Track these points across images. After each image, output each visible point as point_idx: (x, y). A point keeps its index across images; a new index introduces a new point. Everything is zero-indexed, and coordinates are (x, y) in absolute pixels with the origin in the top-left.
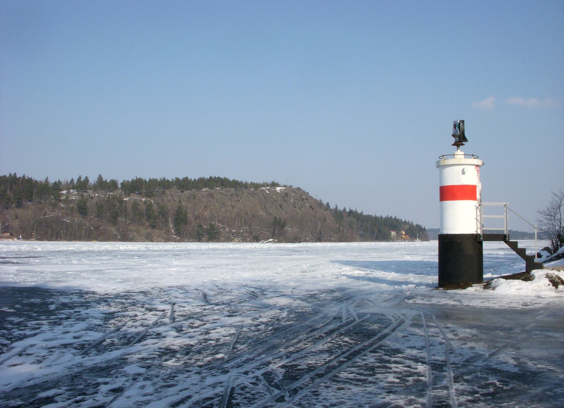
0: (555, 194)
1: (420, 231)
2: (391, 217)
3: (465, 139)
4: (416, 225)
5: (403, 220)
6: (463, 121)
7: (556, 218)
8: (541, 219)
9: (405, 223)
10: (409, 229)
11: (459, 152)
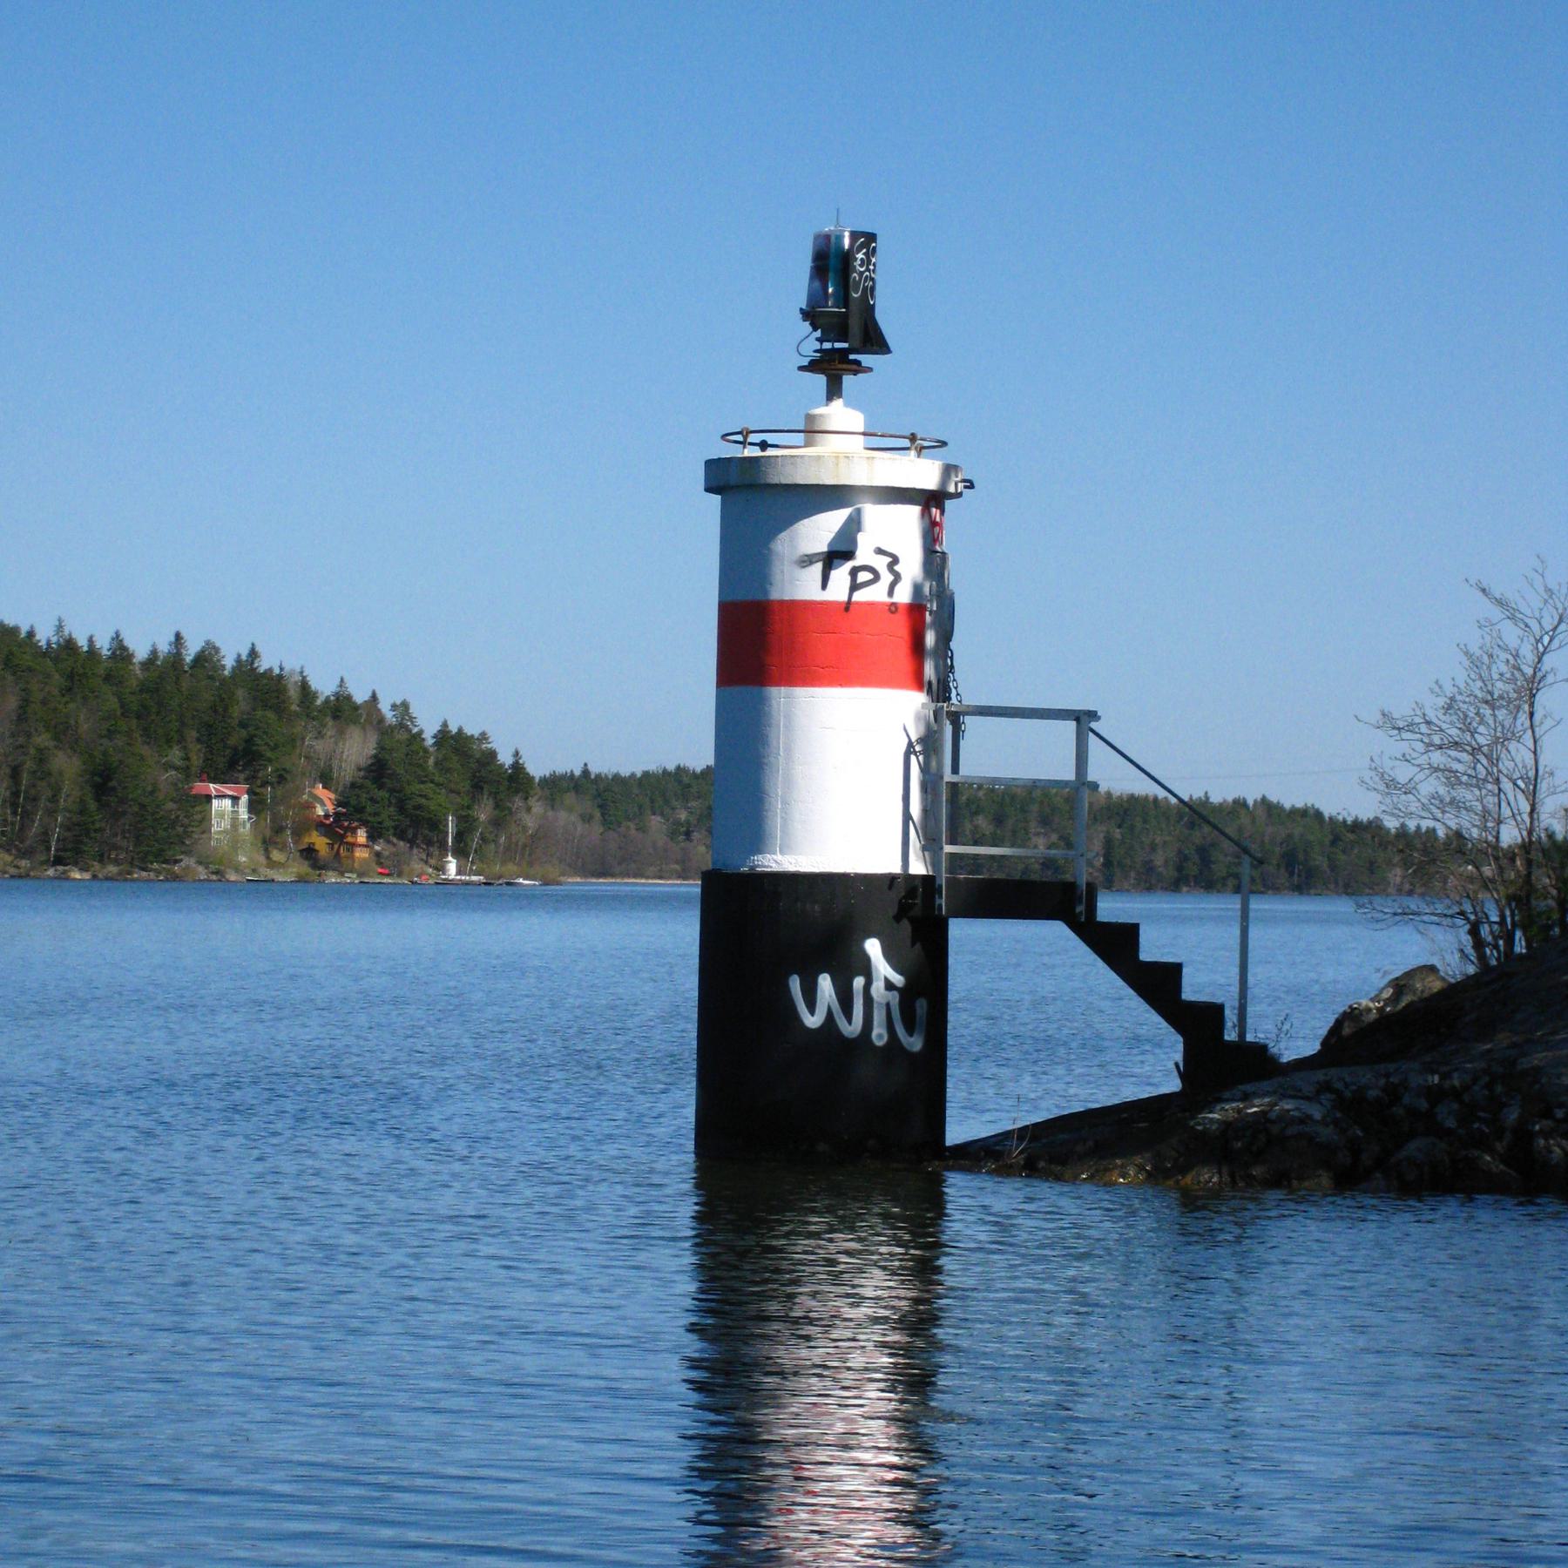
0: (1500, 603)
1: (477, 786)
2: (207, 657)
3: (875, 341)
4: (443, 736)
5: (324, 686)
6: (871, 237)
7: (1506, 765)
8: (1403, 773)
9: (342, 709)
10: (378, 770)
11: (840, 415)
